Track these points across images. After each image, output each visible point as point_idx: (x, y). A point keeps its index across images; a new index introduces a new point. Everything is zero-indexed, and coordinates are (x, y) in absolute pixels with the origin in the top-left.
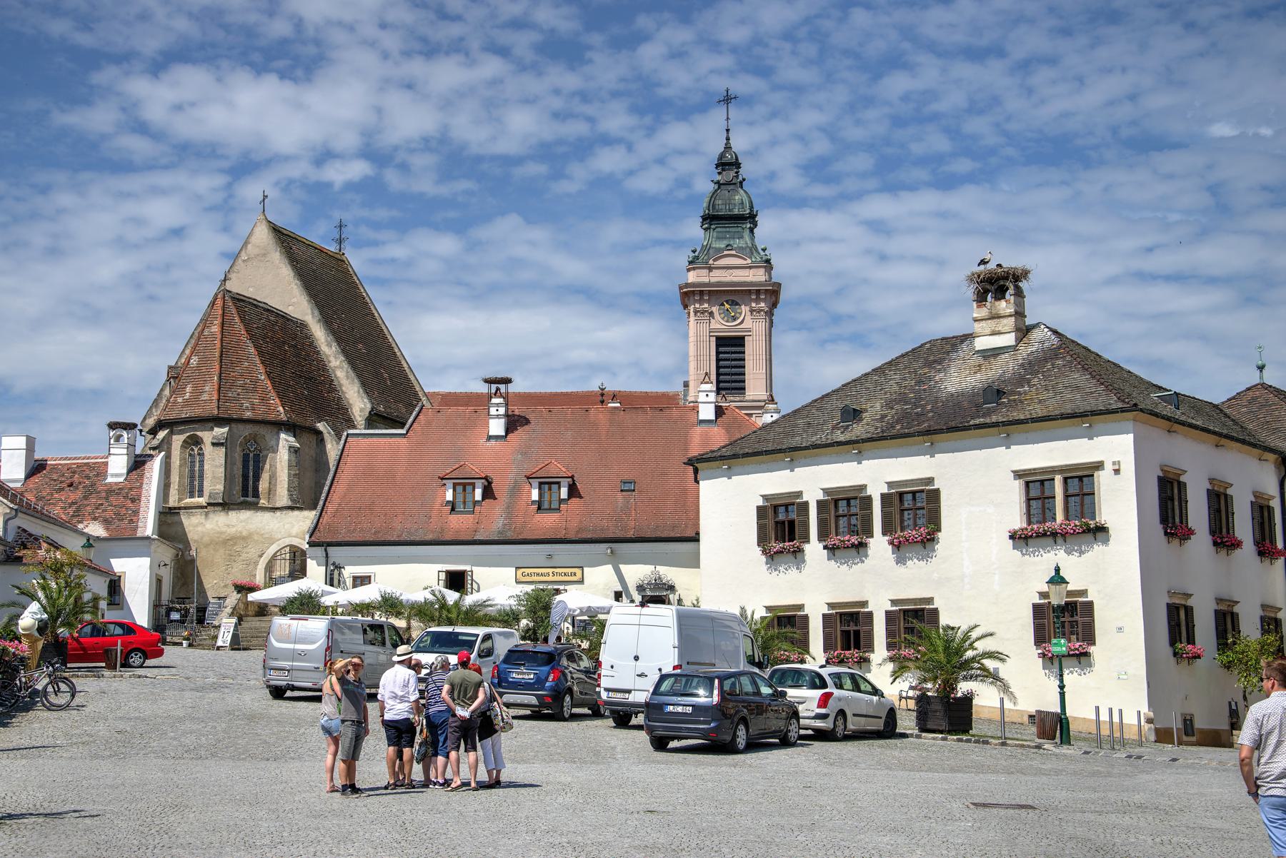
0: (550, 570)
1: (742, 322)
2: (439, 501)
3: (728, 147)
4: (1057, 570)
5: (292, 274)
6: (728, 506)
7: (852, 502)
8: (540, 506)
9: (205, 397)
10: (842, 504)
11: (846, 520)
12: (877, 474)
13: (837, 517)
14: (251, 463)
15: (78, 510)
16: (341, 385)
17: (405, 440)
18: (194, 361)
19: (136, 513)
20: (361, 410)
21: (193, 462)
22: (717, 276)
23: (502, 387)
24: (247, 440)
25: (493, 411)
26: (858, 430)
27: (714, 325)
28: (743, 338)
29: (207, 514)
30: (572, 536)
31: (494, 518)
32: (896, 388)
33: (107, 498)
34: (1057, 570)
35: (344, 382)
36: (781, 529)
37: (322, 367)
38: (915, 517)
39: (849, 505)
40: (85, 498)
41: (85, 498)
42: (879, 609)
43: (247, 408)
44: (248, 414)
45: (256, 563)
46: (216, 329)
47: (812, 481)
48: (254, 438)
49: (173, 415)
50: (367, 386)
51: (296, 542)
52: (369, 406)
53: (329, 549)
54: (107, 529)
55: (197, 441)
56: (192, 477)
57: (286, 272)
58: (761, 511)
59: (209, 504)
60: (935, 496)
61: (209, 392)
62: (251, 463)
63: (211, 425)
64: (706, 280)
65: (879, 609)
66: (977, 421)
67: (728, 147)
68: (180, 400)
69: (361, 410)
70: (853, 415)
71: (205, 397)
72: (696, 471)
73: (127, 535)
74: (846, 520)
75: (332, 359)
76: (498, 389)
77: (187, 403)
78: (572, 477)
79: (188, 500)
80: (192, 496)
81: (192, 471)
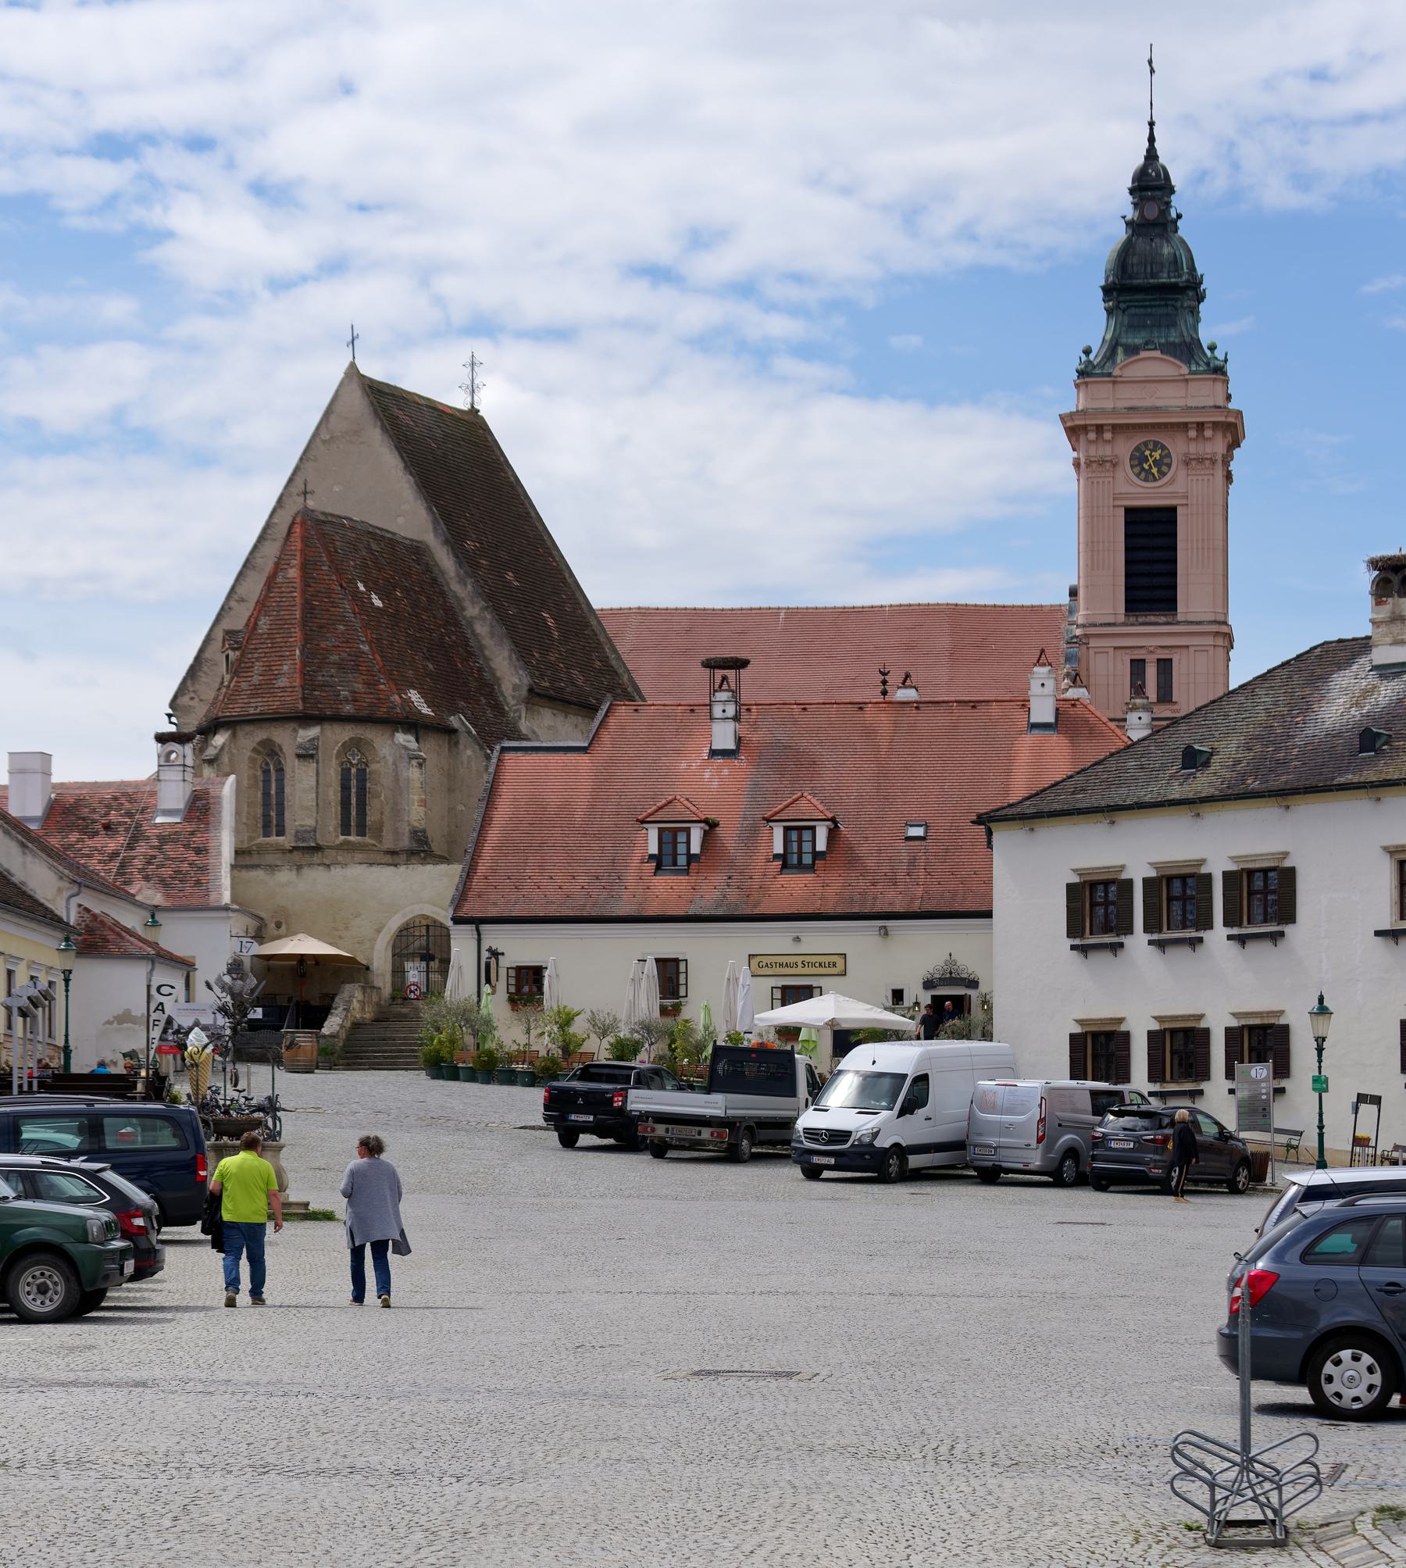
0: (799, 959)
1: (1172, 481)
2: (638, 854)
3: (1151, 155)
4: (1321, 999)
5: (401, 465)
6: (1032, 880)
7: (1189, 881)
8: (785, 862)
9: (283, 682)
10: (1177, 884)
11: (1179, 903)
12: (1220, 844)
13: (1170, 900)
14: (354, 782)
15: (122, 866)
16: (482, 648)
17: (584, 758)
18: (264, 624)
19: (204, 869)
20: (515, 688)
21: (267, 782)
22: (1129, 396)
23: (731, 674)
24: (346, 747)
25: (717, 711)
26: (1203, 783)
27: (1123, 488)
28: (1173, 510)
29: (299, 868)
30: (829, 909)
31: (710, 891)
32: (1262, 716)
33: (159, 848)
34: (1321, 999)
35: (487, 642)
36: (1096, 912)
37: (452, 616)
38: (1265, 899)
39: (1184, 885)
40: (130, 847)
41: (130, 847)
42: (1218, 1026)
43: (347, 700)
44: (348, 709)
45: (373, 940)
46: (293, 573)
47: (1138, 850)
48: (356, 744)
49: (235, 711)
50: (523, 652)
51: (429, 910)
52: (526, 681)
53: (483, 927)
54: (167, 896)
55: (270, 751)
56: (266, 804)
57: (390, 462)
58: (1071, 888)
59: (295, 848)
60: (1288, 876)
61: (288, 675)
62: (354, 782)
63: (293, 725)
64: (1109, 405)
65: (1218, 1026)
66: (1342, 780)
67: (1151, 155)
68: (244, 685)
69: (515, 688)
70: (1193, 759)
71: (283, 682)
72: (990, 833)
73: (195, 902)
74: (1179, 903)
75: (467, 604)
76: (724, 678)
77: (256, 692)
78: (833, 820)
79: (261, 840)
80: (266, 834)
81: (266, 794)
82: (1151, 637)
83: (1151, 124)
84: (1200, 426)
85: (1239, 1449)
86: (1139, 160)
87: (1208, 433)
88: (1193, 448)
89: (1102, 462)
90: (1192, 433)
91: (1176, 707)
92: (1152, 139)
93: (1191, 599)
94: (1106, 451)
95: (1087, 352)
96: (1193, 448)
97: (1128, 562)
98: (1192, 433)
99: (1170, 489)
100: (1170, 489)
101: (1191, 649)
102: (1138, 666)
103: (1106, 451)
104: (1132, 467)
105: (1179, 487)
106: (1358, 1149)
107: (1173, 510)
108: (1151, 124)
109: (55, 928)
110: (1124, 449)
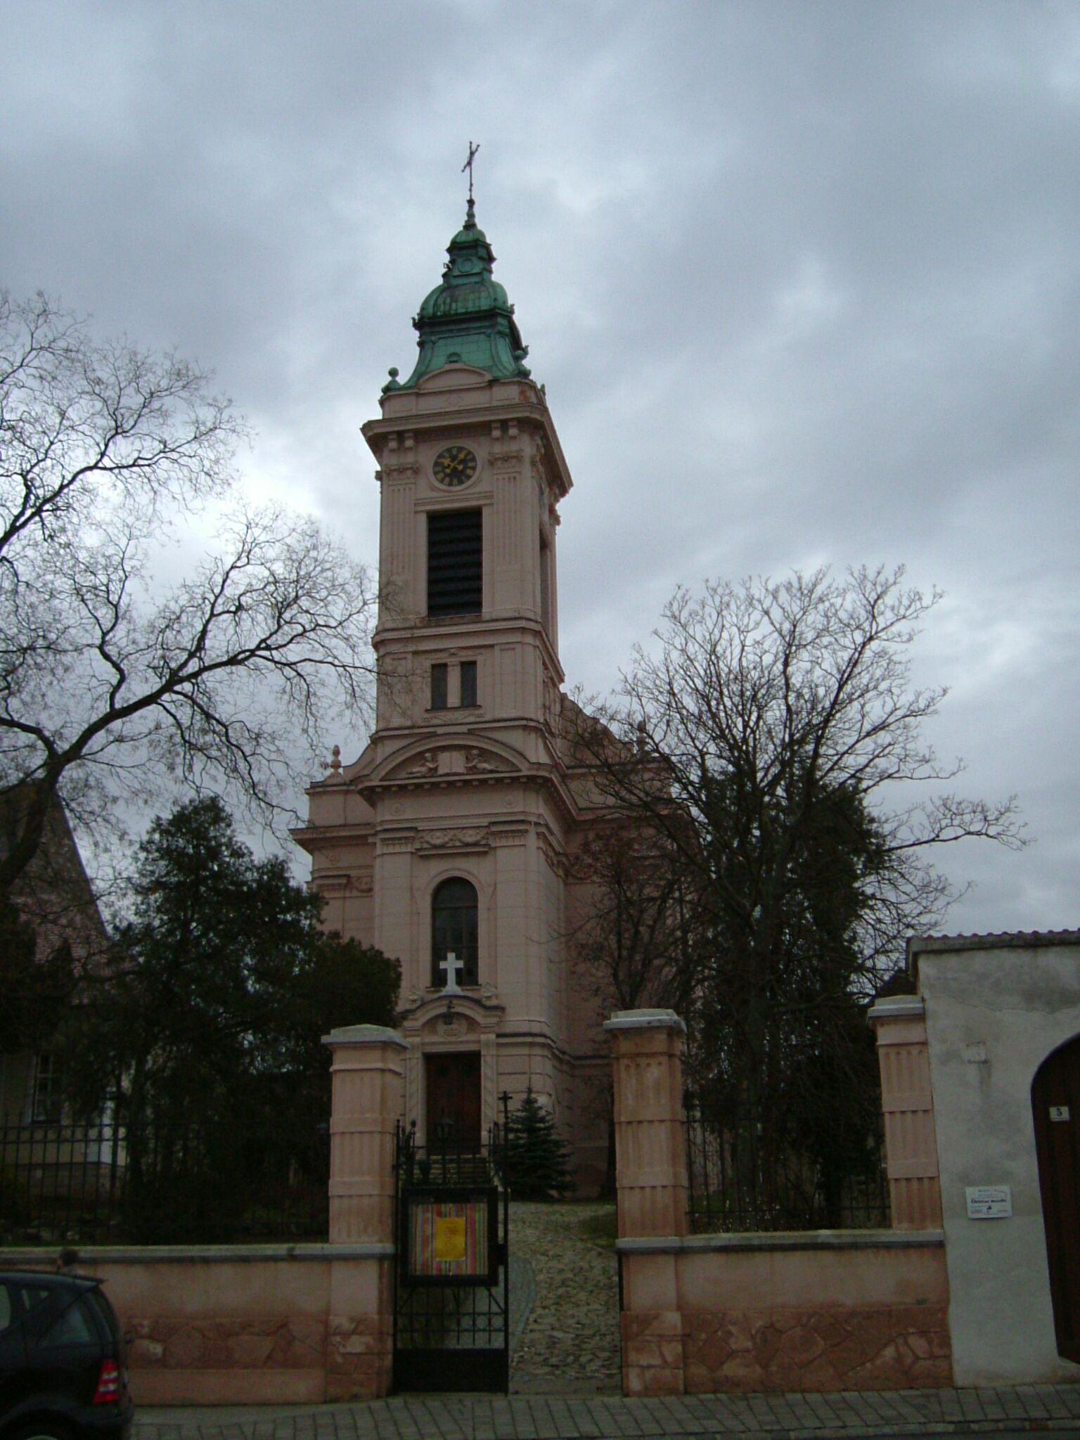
1: (479, 480)
3: (470, 226)
67: (470, 226)
82: (453, 638)
83: (471, 203)
84: (504, 424)
85: (117, 706)
86: (459, 227)
87: (513, 431)
88: (498, 449)
89: (401, 470)
90: (496, 433)
91: (481, 711)
92: (471, 215)
93: (501, 593)
94: (409, 458)
95: (393, 373)
96: (498, 449)
97: (432, 544)
98: (496, 433)
99: (477, 489)
100: (477, 489)
101: (497, 649)
102: (439, 670)
103: (513, 447)
104: (436, 473)
105: (483, 487)
106: (498, 1342)
107: (476, 513)
108: (471, 203)
109: (490, 1267)
110: (427, 456)
